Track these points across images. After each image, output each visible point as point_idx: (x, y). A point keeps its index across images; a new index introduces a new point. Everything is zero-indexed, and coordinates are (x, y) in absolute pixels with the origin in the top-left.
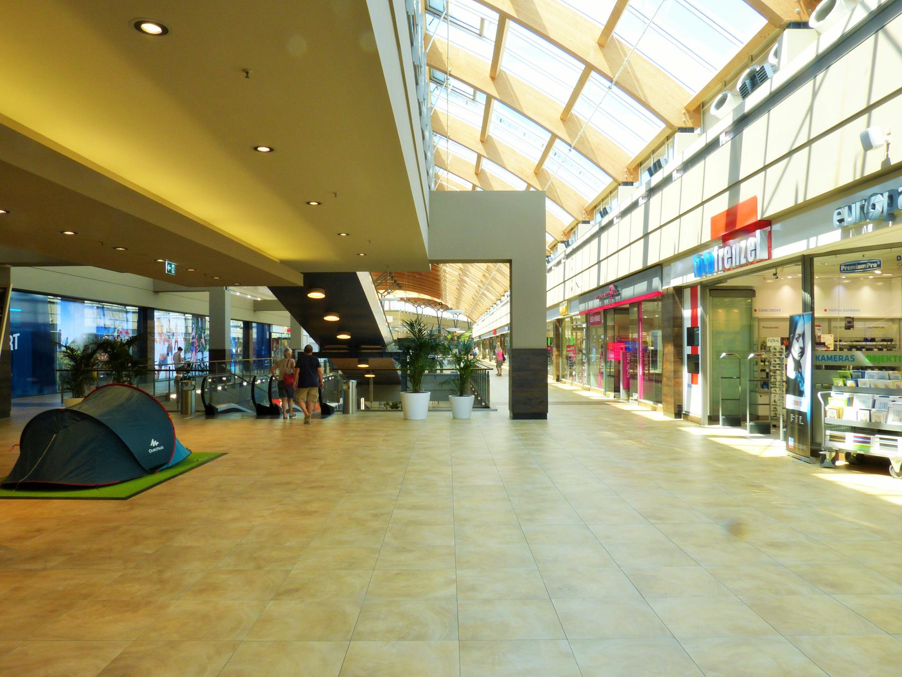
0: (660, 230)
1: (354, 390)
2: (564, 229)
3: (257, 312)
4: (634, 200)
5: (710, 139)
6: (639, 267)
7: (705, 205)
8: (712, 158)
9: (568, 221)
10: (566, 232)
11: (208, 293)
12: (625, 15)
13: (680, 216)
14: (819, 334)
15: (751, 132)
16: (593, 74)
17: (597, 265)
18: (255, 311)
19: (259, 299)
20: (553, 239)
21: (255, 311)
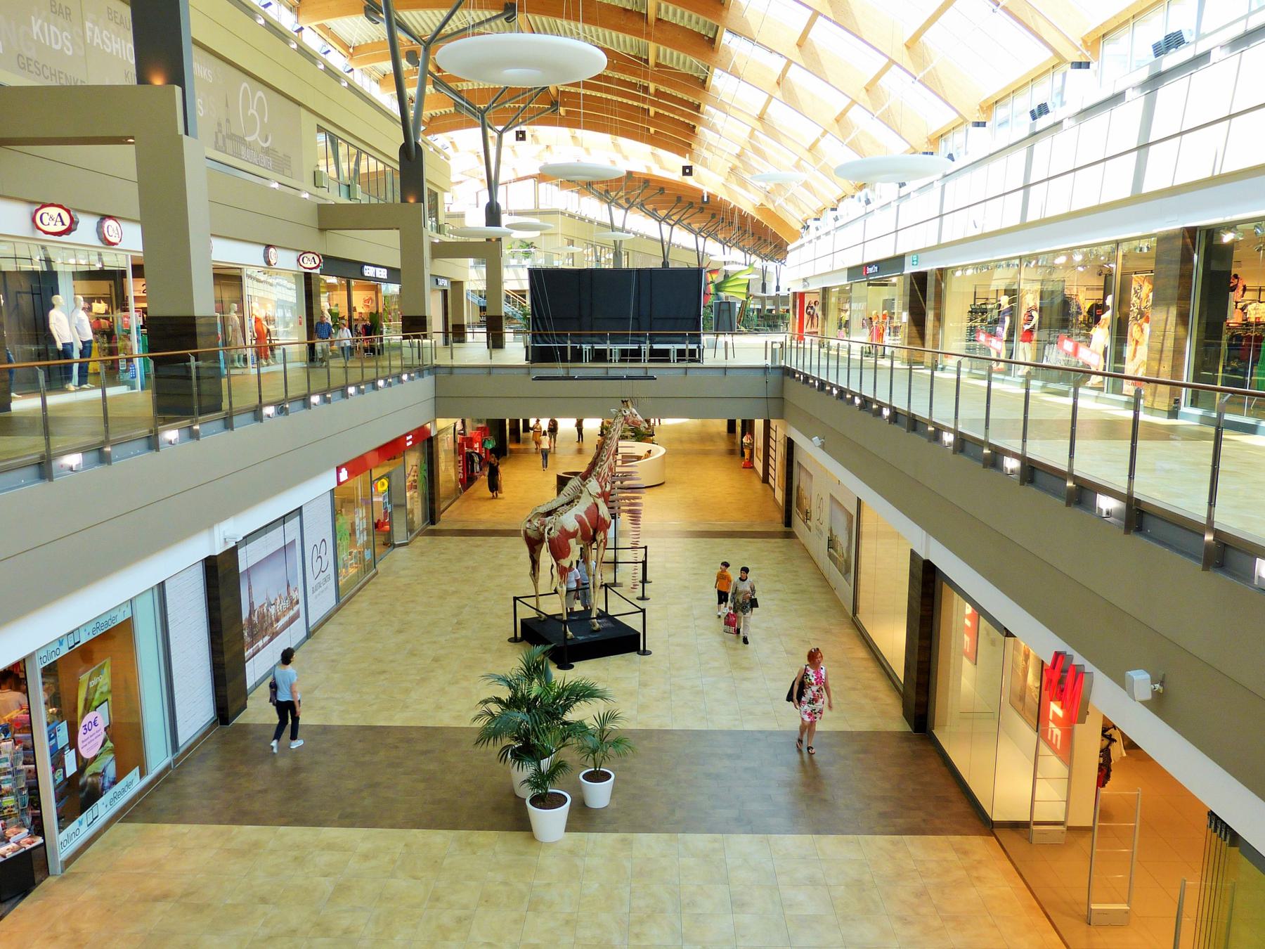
0: (1228, 121)
1: (18, 461)
2: (982, 100)
3: (328, 233)
4: (1117, 91)
5: (1199, 52)
6: (935, 243)
7: (1234, 120)
8: (1119, 110)
9: (941, 118)
10: (985, 106)
11: (398, 232)
12: (950, 12)
13: (1230, 117)
14: (226, 252)
15: (1165, 92)
16: (894, 67)
17: (1022, 192)
18: (322, 230)
19: (437, 241)
20: (821, 204)
21: (322, 230)
